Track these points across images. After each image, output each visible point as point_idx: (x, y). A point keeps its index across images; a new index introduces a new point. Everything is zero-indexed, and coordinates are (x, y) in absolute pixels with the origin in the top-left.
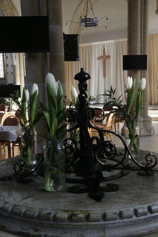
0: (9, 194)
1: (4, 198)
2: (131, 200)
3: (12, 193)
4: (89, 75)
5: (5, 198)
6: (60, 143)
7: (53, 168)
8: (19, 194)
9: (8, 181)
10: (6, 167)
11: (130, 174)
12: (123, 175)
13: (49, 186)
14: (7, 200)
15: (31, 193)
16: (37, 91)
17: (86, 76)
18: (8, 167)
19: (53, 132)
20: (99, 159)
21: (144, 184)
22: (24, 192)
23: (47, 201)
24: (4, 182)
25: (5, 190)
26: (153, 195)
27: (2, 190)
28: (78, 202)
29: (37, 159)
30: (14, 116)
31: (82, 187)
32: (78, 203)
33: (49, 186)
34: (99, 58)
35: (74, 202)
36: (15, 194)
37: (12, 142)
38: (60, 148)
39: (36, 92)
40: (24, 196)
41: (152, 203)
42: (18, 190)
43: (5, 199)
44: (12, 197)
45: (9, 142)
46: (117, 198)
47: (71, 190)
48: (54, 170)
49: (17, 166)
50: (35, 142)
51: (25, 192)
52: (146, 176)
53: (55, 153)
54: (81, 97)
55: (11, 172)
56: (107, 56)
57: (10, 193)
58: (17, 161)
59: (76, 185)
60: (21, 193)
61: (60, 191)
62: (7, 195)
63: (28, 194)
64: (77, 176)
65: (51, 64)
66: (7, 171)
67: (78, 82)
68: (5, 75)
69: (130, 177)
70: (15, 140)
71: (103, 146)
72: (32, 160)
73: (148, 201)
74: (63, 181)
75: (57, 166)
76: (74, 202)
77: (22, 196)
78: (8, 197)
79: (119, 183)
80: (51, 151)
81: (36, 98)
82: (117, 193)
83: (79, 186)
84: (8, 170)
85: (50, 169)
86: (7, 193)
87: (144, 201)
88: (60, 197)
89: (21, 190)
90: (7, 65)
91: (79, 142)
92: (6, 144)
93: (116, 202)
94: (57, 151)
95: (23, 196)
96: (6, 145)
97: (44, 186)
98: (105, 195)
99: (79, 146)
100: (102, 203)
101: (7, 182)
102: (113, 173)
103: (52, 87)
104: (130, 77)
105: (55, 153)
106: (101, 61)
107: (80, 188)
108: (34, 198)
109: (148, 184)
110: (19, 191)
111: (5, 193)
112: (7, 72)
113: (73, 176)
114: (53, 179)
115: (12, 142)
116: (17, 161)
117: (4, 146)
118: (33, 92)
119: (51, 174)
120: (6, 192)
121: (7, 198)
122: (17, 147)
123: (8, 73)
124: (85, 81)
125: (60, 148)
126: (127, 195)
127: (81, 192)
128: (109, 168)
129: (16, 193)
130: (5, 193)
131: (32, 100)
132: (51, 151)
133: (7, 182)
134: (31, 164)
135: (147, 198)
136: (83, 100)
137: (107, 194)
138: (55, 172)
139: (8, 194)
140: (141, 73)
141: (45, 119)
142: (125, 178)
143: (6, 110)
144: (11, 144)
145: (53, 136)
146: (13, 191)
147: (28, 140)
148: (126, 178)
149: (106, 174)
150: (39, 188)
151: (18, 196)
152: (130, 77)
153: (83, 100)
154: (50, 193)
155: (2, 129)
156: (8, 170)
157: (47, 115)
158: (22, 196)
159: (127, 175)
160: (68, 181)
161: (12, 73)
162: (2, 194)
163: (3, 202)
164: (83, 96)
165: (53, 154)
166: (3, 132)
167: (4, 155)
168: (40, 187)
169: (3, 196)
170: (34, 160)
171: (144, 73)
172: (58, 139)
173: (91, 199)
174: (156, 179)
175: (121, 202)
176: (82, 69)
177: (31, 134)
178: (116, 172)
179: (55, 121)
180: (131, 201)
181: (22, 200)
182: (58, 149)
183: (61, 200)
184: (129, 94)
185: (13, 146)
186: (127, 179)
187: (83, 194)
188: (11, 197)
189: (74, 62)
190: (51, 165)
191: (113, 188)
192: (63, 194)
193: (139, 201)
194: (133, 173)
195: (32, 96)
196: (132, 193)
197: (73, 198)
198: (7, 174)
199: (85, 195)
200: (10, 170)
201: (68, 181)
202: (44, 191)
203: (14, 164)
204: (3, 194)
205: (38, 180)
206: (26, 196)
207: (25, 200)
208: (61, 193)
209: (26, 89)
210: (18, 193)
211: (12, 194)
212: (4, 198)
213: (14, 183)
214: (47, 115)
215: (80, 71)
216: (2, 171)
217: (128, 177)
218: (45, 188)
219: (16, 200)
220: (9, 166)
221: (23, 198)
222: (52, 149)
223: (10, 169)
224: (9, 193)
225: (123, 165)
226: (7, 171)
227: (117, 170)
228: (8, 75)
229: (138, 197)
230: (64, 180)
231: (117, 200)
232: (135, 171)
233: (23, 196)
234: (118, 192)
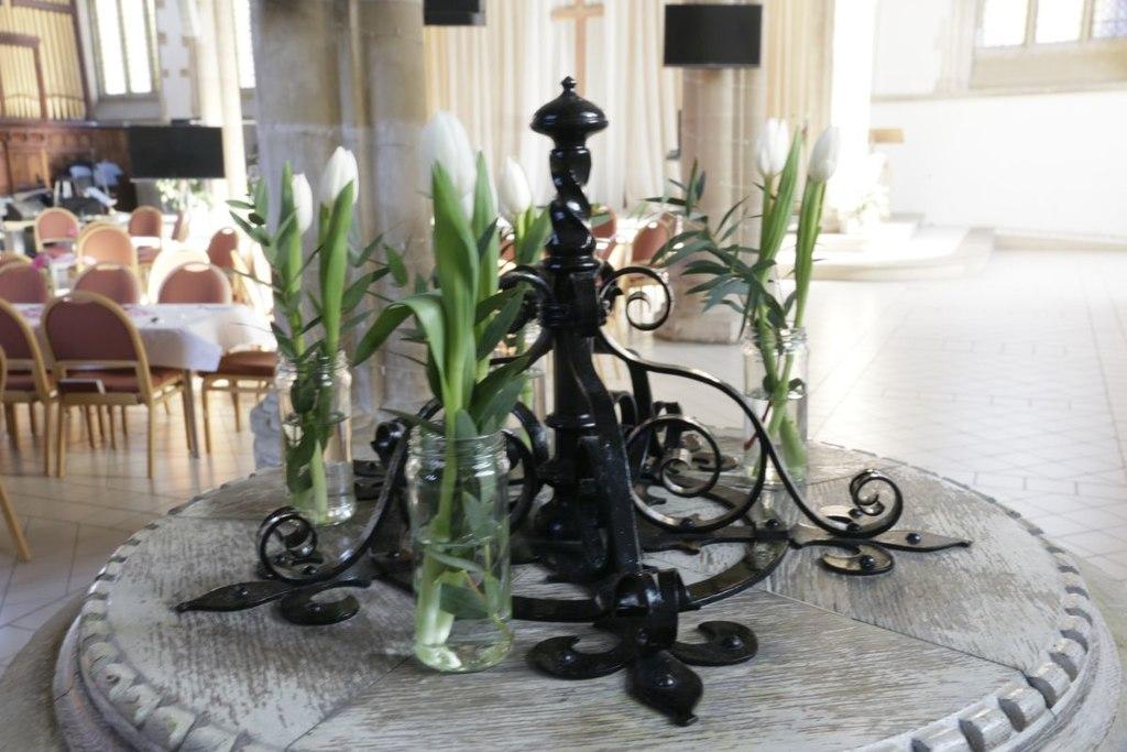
0: (251, 691)
1: (232, 714)
2: (830, 709)
3: (265, 681)
4: (600, 114)
5: (239, 709)
6: (489, 449)
7: (458, 563)
8: (299, 686)
9: (236, 614)
10: (215, 536)
11: (786, 568)
12: (760, 575)
13: (435, 637)
14: (246, 723)
15: (357, 679)
16: (350, 185)
17: (590, 115)
18: (227, 537)
19: (456, 397)
20: (634, 487)
21: (863, 618)
22: (323, 677)
23: (439, 723)
24: (218, 621)
25: (228, 662)
26: (922, 677)
27: (218, 666)
28: (591, 729)
29: (362, 496)
30: (202, 263)
31: (591, 642)
32: (592, 734)
33: (435, 637)
34: (557, 13)
35: (571, 730)
36: (279, 684)
37: (202, 374)
38: (491, 473)
39: (344, 194)
40: (327, 696)
41: (925, 722)
42: (290, 662)
43: (239, 718)
44: (272, 704)
45: (187, 373)
46: (763, 699)
47: (547, 661)
48: (454, 570)
49: (273, 538)
50: (342, 418)
51: (327, 674)
52: (860, 578)
53: (467, 495)
54: (560, 215)
55: (242, 563)
56: (593, 6)
57: (255, 684)
58: (275, 519)
59: (556, 631)
60: (308, 680)
61: (493, 669)
62: (241, 693)
63: (341, 685)
64: (550, 580)
65: (366, 40)
66: (221, 559)
67: (546, 144)
68: (153, 82)
69: (789, 581)
70: (213, 366)
71: (650, 431)
72: (334, 498)
73: (904, 714)
74: (501, 615)
75: (470, 554)
76: (571, 730)
77: (316, 701)
78: (250, 705)
79: (751, 616)
80: (446, 490)
81: (348, 216)
82: (755, 671)
83: (574, 640)
84: (227, 554)
85: (444, 568)
86: (240, 681)
87: (891, 713)
88: (497, 699)
89: (304, 661)
90: (162, 37)
91: (550, 421)
92: (174, 380)
93: (765, 725)
94: (475, 486)
95: (321, 697)
96: (178, 384)
97: (414, 642)
98: (705, 682)
99: (547, 435)
100: (701, 732)
101: (231, 615)
102: (710, 561)
103: (454, 181)
104: (780, 122)
105: (467, 495)
106: (567, 26)
107: (579, 646)
108: (376, 708)
109: (881, 621)
110: (295, 669)
111: (230, 681)
112: (164, 67)
113: (531, 581)
114: (450, 612)
115: (202, 374)
116: (275, 519)
117: (164, 393)
118: (335, 192)
119: (445, 587)
120: (236, 675)
121: (247, 712)
122: (218, 394)
123: (165, 73)
124: (582, 140)
125: (491, 473)
126: (804, 683)
127: (586, 668)
128: (688, 536)
129: (283, 684)
130: (230, 681)
131: (327, 223)
132: (446, 490)
133: (234, 619)
134: (328, 518)
135: (900, 699)
136: (569, 225)
137: (714, 678)
138: (459, 581)
139: (245, 687)
140: (737, 80)
141: (420, 336)
142: (769, 589)
143: (167, 229)
144: (197, 383)
145: (457, 417)
146: (267, 668)
147: (310, 413)
148: (773, 589)
149: (692, 569)
150: (390, 651)
151: (294, 697)
152: (780, 122)
153: (569, 225)
154: (447, 679)
155: (154, 320)
156: (227, 554)
157: (429, 315)
158: (316, 701)
159: (777, 570)
160: (525, 609)
161: (184, 72)
162: (219, 690)
163: (232, 733)
164: (568, 212)
165: (457, 497)
166: (158, 333)
167: (168, 426)
168: (394, 645)
169: (224, 700)
170: (343, 499)
171: (750, 81)
172: (480, 431)
173: (643, 711)
174: (907, 589)
175: (789, 723)
176: (567, 84)
177: (328, 384)
178: (725, 556)
179: (467, 343)
180: (829, 718)
181: (322, 721)
182: (478, 475)
183: (508, 720)
184: (772, 202)
185: (206, 388)
186: (781, 592)
187: (598, 680)
188: (264, 704)
189: (464, 30)
190: (448, 552)
191: (732, 644)
192: (508, 685)
193: (867, 713)
194: (798, 560)
195: (330, 205)
196: (824, 671)
197: (558, 706)
198: (224, 576)
199: (609, 689)
200: (236, 551)
201: (525, 609)
202: (412, 666)
203: (263, 532)
204: (224, 689)
205: (379, 604)
206: (334, 699)
207: (335, 721)
208: (498, 675)
209: (298, 173)
210: (293, 682)
211: (266, 692)
212: (232, 714)
213: (263, 618)
214: (429, 315)
215: (561, 90)
216: (198, 556)
217: (784, 582)
218: (418, 650)
219: (292, 724)
220: (229, 529)
221: (322, 707)
222: (450, 478)
223: (236, 546)
224: (251, 680)
225: (749, 522)
226: (221, 559)
227: (725, 544)
228: (165, 81)
229: (856, 692)
230: (508, 613)
231: (764, 710)
232: (808, 549)
233: (321, 697)
234: (758, 667)
